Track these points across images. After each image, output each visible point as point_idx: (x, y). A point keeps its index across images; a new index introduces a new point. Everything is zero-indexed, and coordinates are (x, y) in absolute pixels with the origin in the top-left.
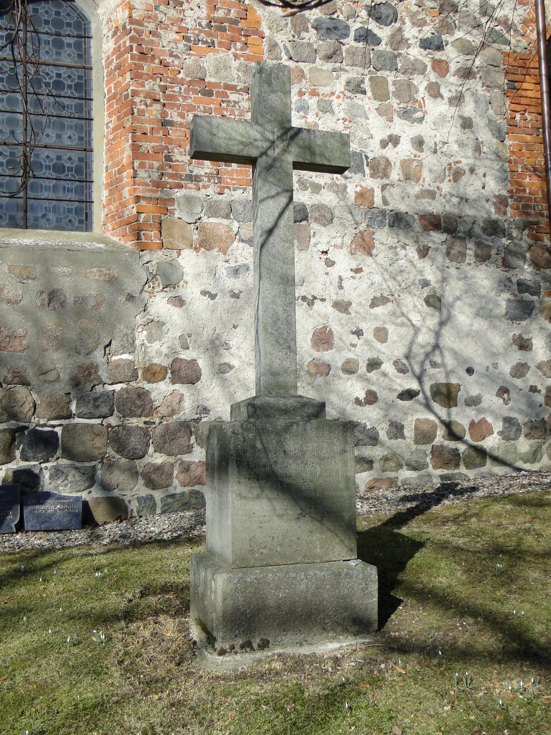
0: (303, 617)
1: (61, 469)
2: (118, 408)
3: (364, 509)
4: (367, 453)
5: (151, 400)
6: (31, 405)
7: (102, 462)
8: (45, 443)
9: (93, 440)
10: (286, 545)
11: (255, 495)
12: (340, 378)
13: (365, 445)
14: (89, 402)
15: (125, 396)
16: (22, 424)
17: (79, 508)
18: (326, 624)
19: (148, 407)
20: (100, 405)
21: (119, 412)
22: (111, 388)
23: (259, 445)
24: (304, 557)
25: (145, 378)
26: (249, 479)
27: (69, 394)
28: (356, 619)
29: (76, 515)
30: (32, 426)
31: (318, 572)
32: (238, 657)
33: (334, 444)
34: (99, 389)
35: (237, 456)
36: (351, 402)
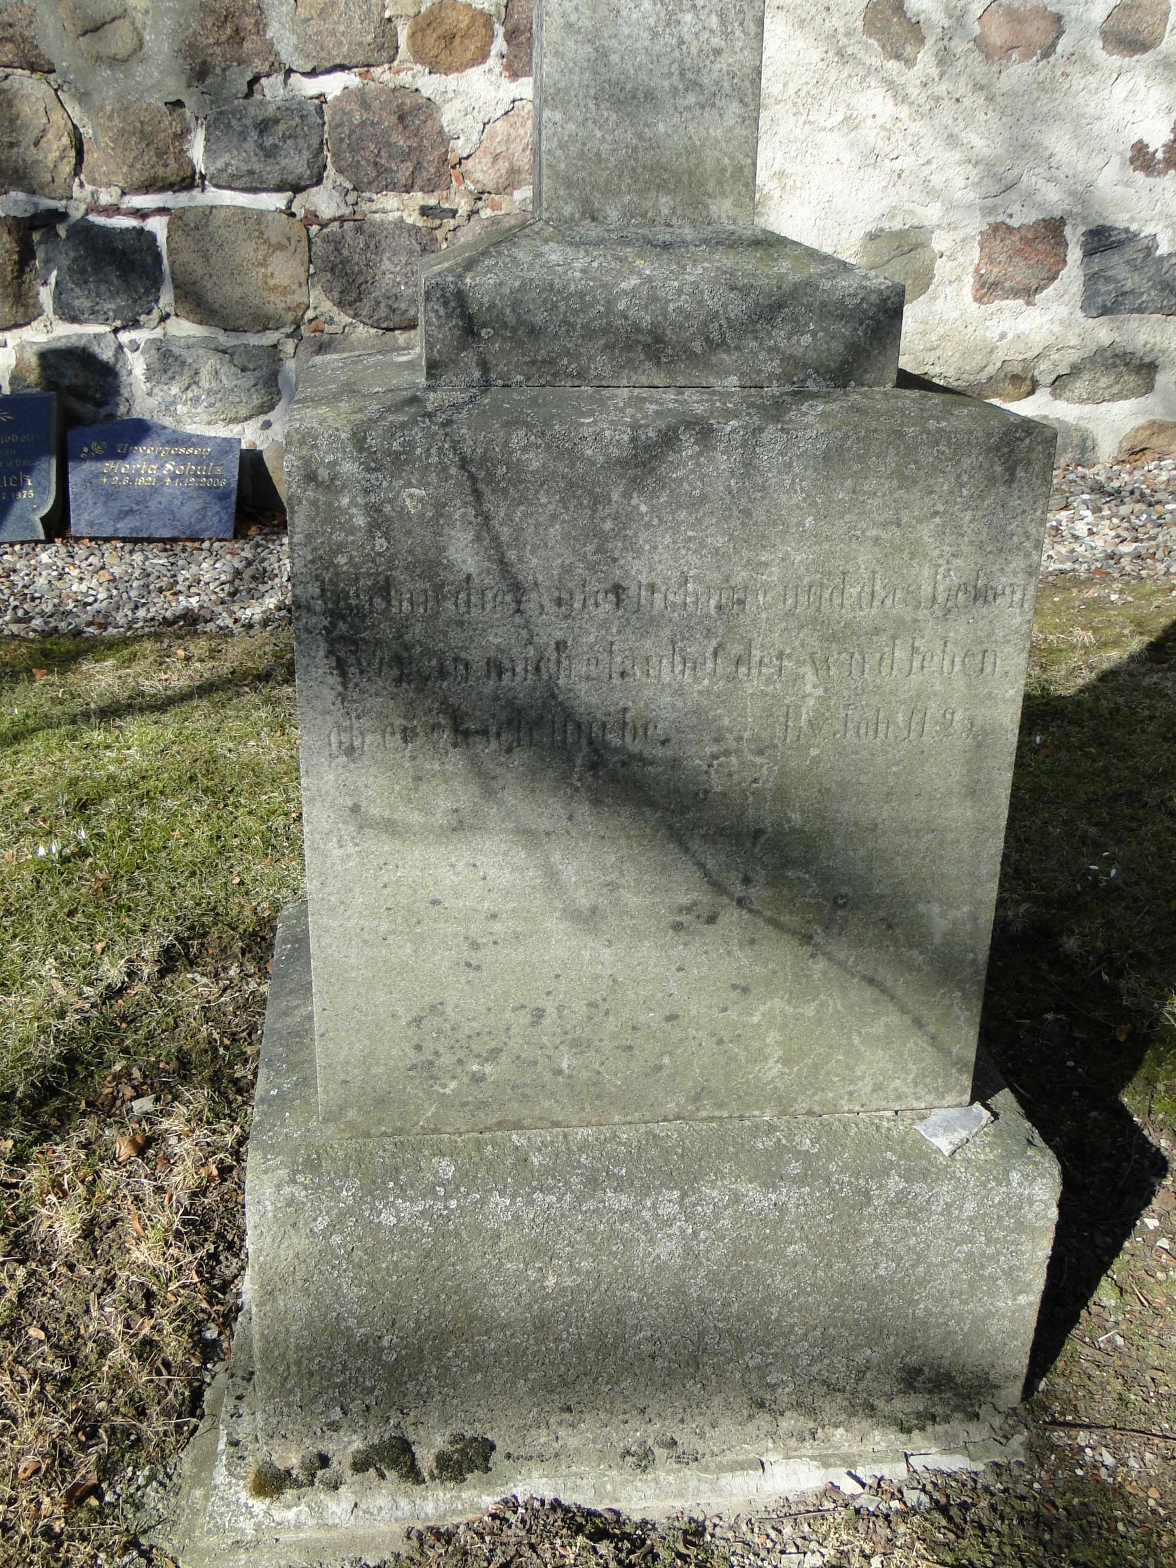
0: (659, 1363)
1: (175, 350)
2: (337, 156)
3: (1099, 542)
4: (1142, 338)
5: (441, 132)
6: (65, 140)
7: (295, 334)
8: (121, 266)
9: (264, 264)
10: (607, 1046)
11: (440, 819)
12: (1092, 68)
13: (1140, 310)
14: (243, 136)
15: (357, 119)
16: (46, 203)
17: (229, 474)
18: (773, 1387)
19: (434, 156)
20: (281, 144)
21: (340, 171)
22: (310, 87)
23: (464, 554)
24: (696, 1098)
25: (419, 55)
26: (407, 734)
27: (179, 104)
28: (919, 1371)
29: (222, 496)
30: (76, 213)
31: (750, 1190)
32: (338, 1506)
33: (916, 551)
34: (272, 89)
35: (335, 614)
36: (1116, 160)
